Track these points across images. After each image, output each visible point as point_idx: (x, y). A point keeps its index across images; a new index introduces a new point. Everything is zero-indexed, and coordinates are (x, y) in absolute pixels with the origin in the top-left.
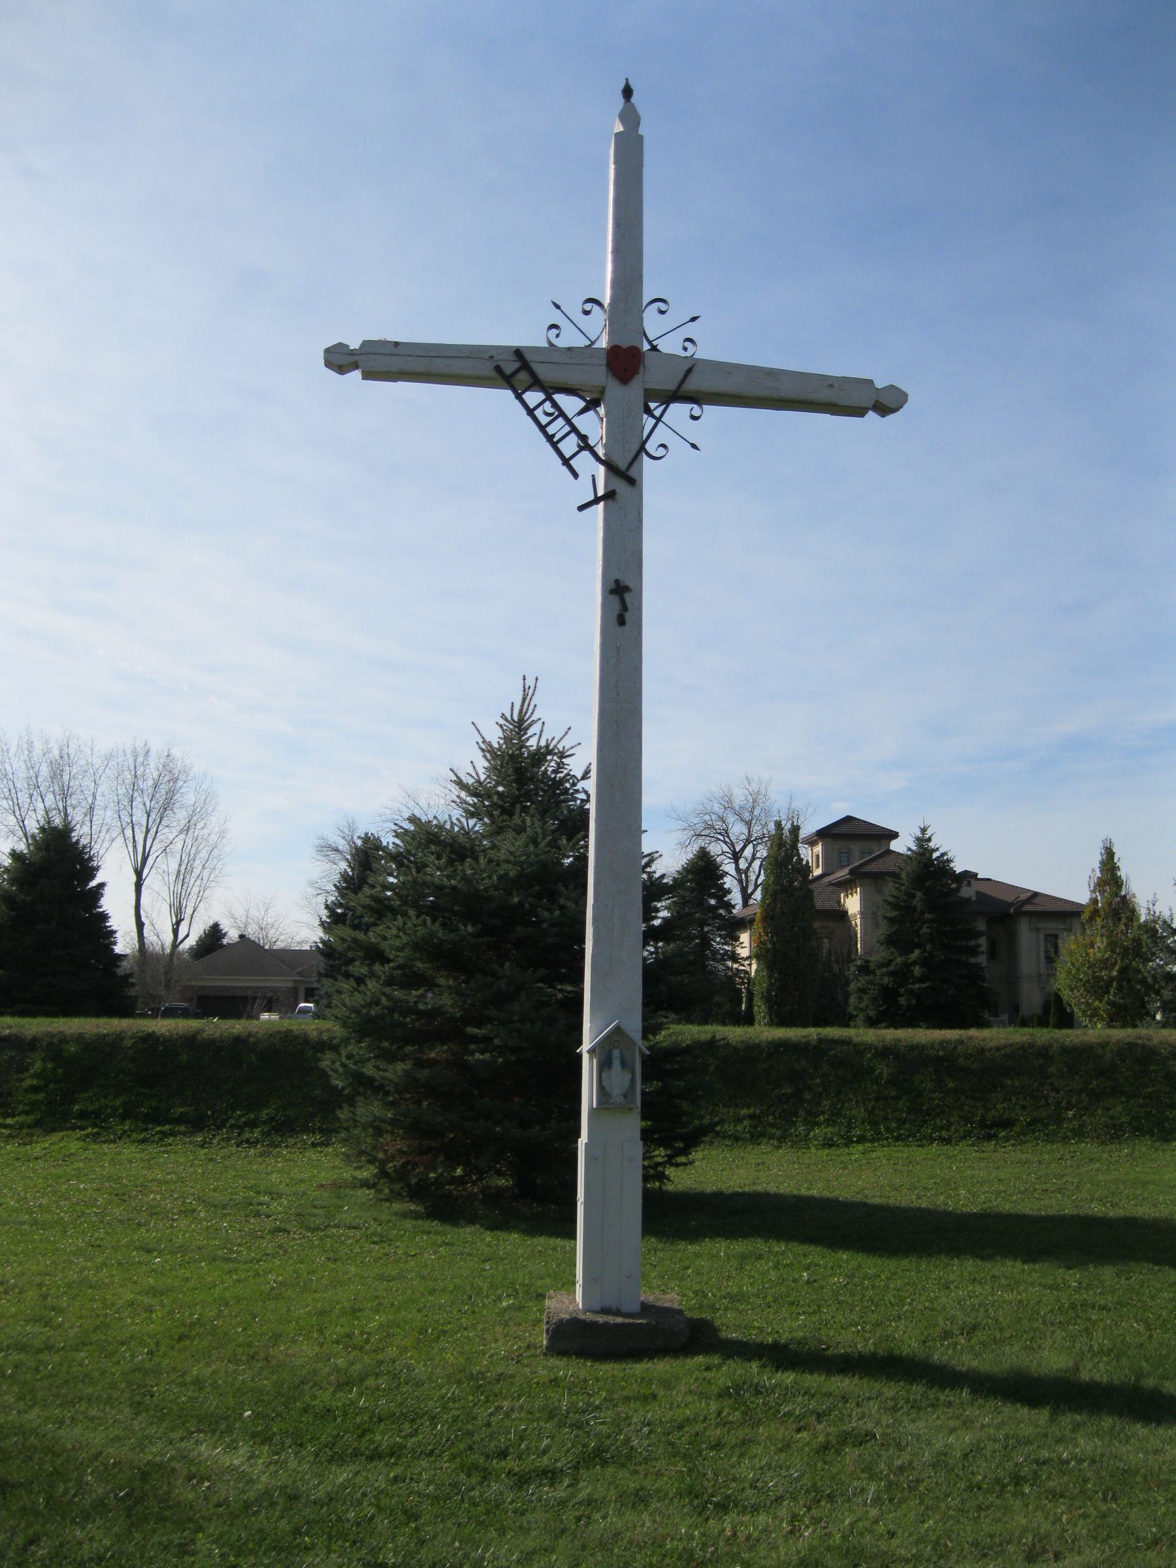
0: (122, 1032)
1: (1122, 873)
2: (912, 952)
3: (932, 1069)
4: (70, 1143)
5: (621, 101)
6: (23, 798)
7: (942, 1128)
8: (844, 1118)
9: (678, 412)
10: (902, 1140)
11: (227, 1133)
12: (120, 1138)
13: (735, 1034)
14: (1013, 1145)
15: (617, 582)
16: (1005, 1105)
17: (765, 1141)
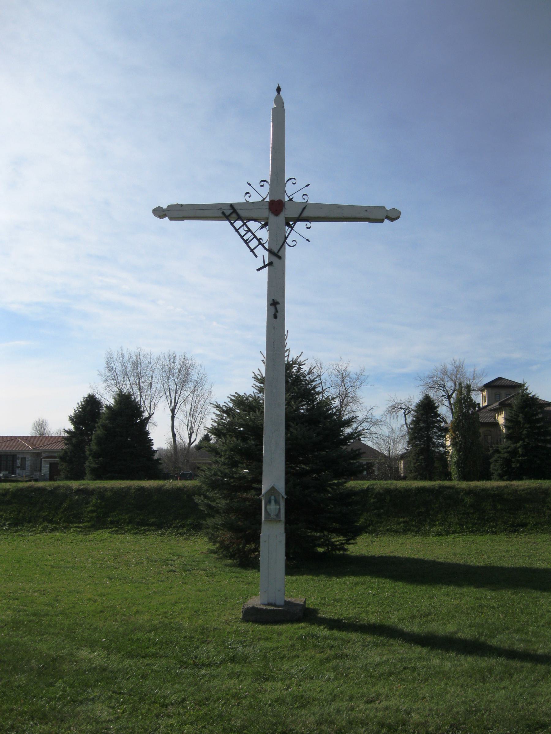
0: (130, 486)
2: (519, 442)
4: (104, 534)
5: (276, 93)
6: (120, 379)
7: (493, 527)
8: (448, 522)
9: (300, 226)
10: (473, 533)
11: (172, 530)
12: (126, 532)
13: (447, 483)
14: (525, 535)
15: (273, 300)
16: (524, 516)
17: (409, 533)
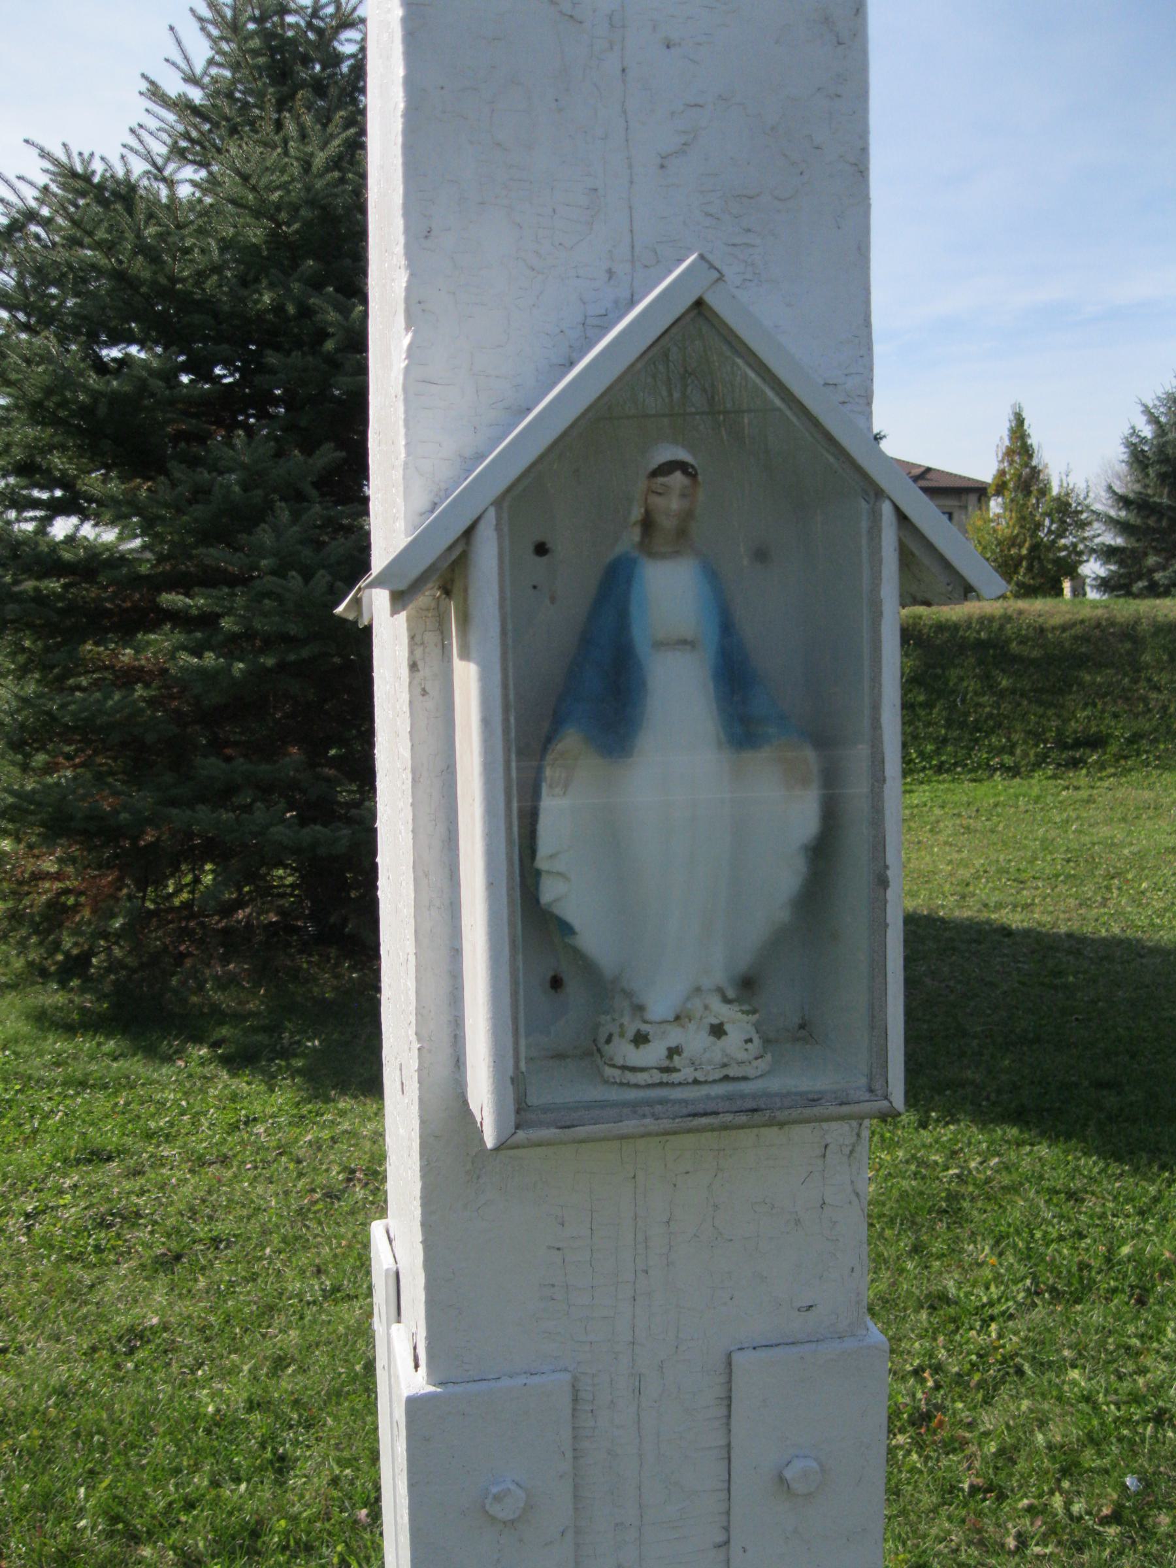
1: (1033, 441)
3: (972, 660)
7: (1001, 750)
10: (948, 771)
16: (1087, 713)
